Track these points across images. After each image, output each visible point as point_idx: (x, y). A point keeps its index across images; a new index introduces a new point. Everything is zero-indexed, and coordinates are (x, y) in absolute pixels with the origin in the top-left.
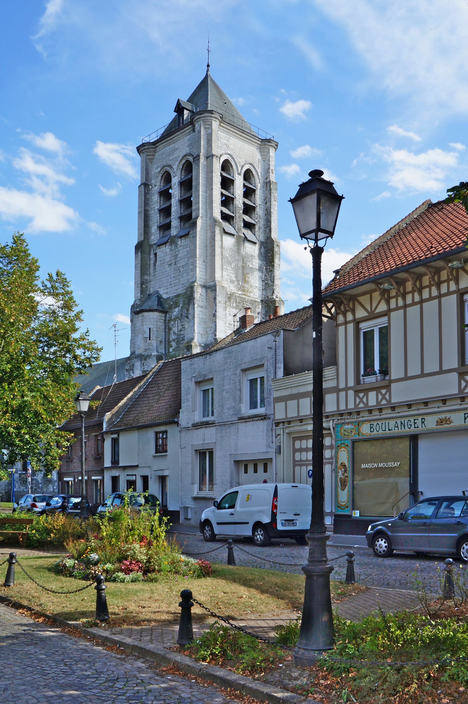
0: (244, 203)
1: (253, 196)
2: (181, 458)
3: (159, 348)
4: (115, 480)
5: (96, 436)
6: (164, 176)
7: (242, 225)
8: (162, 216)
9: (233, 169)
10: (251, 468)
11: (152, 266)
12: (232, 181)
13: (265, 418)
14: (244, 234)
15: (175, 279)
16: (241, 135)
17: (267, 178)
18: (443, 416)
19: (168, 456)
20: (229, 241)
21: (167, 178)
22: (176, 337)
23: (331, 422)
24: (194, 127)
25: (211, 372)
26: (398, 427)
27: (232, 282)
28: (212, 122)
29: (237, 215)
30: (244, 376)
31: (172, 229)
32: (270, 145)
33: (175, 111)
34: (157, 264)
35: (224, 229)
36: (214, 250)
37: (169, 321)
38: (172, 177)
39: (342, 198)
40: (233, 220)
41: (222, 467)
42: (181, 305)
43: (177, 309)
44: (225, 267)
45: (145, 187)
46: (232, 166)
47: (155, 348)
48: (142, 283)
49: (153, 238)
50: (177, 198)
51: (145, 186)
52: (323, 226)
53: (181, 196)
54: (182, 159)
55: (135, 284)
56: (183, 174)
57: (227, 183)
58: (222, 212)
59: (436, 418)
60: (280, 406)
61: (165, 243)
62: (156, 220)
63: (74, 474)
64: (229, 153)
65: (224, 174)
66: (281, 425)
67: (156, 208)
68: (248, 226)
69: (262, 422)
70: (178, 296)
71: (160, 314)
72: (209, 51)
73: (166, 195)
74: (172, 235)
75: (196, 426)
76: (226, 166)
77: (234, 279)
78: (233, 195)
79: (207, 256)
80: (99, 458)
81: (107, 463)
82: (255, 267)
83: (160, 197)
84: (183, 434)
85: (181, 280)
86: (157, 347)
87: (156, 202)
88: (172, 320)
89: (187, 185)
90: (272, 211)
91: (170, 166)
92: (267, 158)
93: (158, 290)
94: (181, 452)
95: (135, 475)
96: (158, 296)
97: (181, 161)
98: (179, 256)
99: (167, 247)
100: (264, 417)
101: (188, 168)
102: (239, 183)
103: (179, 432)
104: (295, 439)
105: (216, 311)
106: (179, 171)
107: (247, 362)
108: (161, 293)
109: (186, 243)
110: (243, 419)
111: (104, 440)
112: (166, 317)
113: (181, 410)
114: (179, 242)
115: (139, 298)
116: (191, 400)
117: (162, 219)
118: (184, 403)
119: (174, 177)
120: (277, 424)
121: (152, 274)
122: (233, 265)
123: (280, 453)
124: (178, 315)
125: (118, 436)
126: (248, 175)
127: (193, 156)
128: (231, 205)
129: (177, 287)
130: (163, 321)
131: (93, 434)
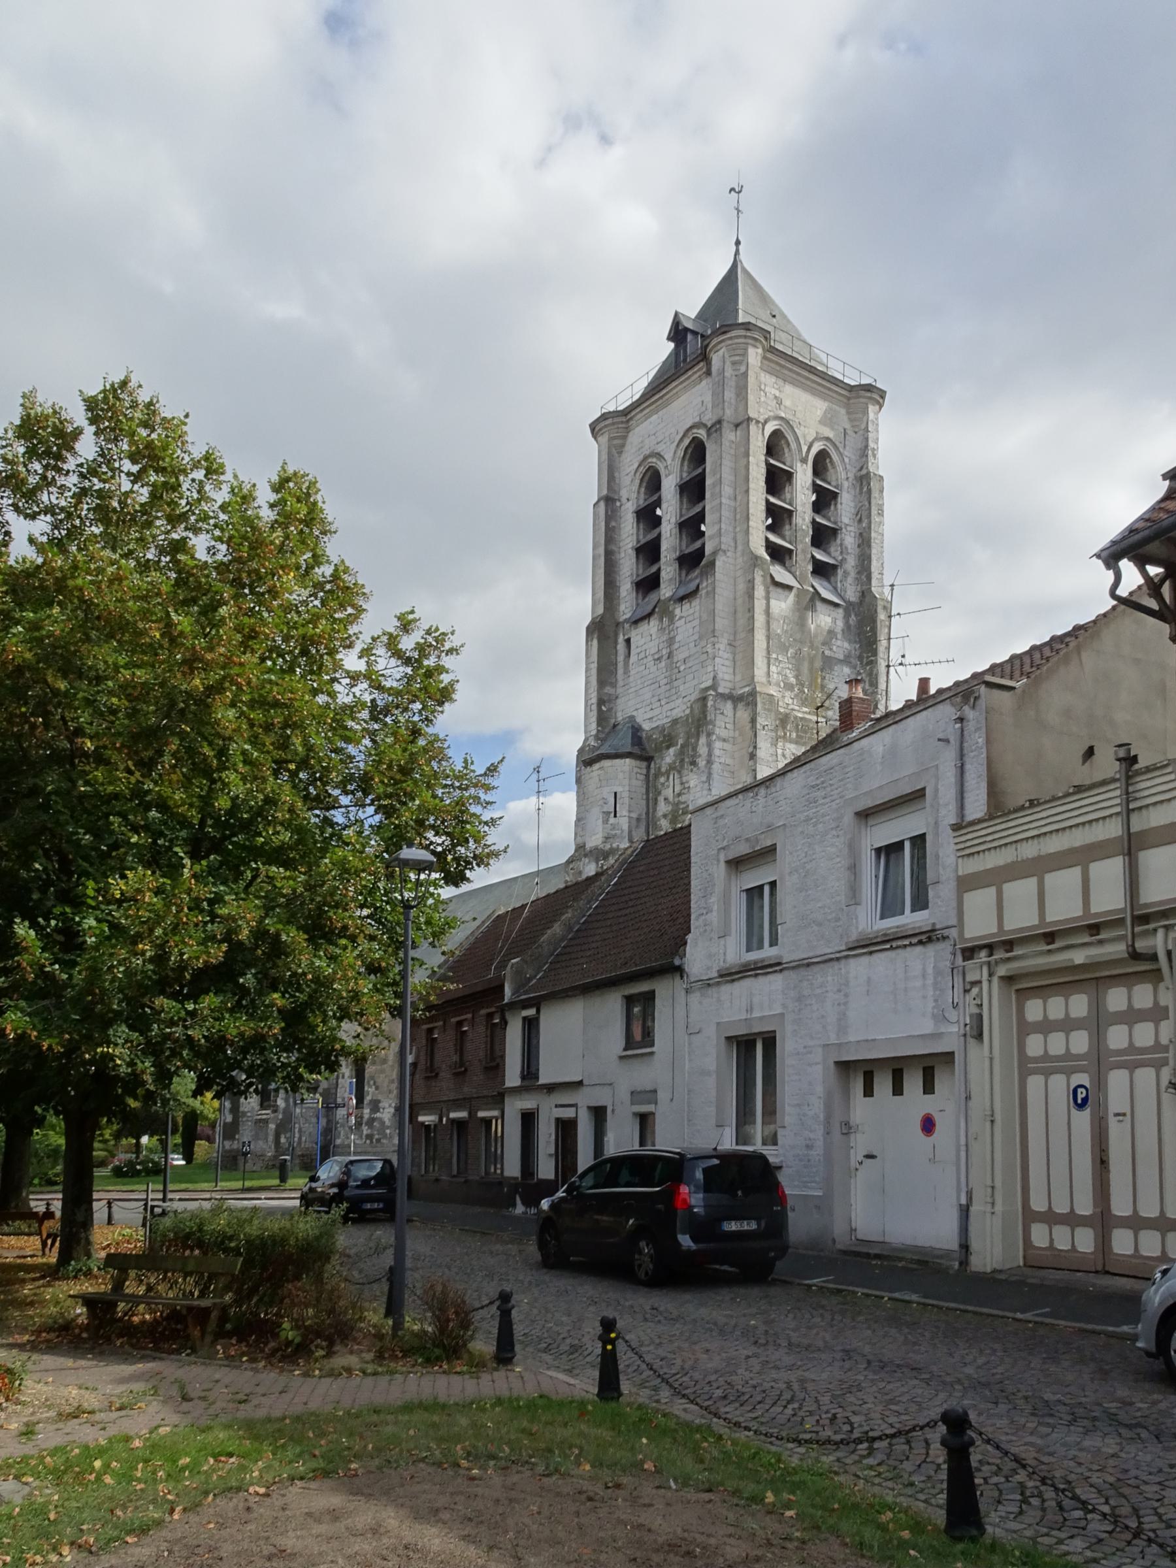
0: (814, 522)
1: (832, 507)
2: (690, 1060)
3: (634, 833)
4: (529, 1120)
5: (490, 1016)
6: (647, 478)
7: (810, 568)
8: (641, 561)
9: (790, 450)
10: (883, 1085)
11: (620, 665)
12: (789, 476)
13: (930, 940)
14: (813, 586)
15: (668, 687)
16: (808, 379)
17: (861, 468)
19: (656, 1057)
20: (782, 605)
21: (652, 481)
22: (670, 808)
23: (1160, 934)
24: (709, 364)
25: (770, 829)
27: (789, 687)
28: (746, 349)
29: (800, 547)
30: (863, 832)
31: (662, 586)
32: (870, 398)
33: (669, 339)
34: (632, 660)
35: (772, 577)
36: (752, 618)
37: (656, 776)
38: (663, 477)
40: (791, 558)
41: (803, 1077)
42: (680, 741)
43: (672, 751)
44: (774, 656)
45: (606, 506)
46: (788, 445)
47: (626, 834)
48: (601, 702)
49: (622, 607)
50: (673, 520)
51: (609, 501)
53: (681, 516)
54: (684, 436)
56: (686, 468)
58: (767, 539)
60: (980, 902)
61: (648, 616)
62: (629, 568)
64: (783, 415)
66: (983, 953)
67: (630, 545)
68: (822, 570)
69: (919, 949)
70: (675, 722)
71: (638, 763)
72: (739, 211)
73: (648, 516)
74: (662, 598)
75: (731, 975)
76: (774, 445)
77: (793, 680)
79: (735, 634)
80: (495, 1066)
81: (513, 1078)
82: (836, 656)
83: (638, 522)
84: (695, 998)
85: (681, 688)
86: (630, 832)
87: (629, 533)
88: (663, 775)
89: (694, 489)
90: (873, 535)
91: (659, 456)
92: (863, 427)
93: (634, 713)
94: (690, 1044)
95: (575, 1105)
96: (633, 727)
97: (681, 440)
98: (677, 639)
99: (652, 623)
100: (928, 937)
101: (697, 453)
102: (803, 476)
103: (683, 993)
104: (1024, 994)
105: (755, 747)
106: (678, 462)
107: (878, 784)
108: (638, 720)
109: (691, 611)
110: (869, 945)
111: (506, 1023)
112: (648, 768)
113: (689, 938)
114: (677, 611)
115: (594, 732)
116: (715, 908)
117: (641, 566)
118: (697, 919)
119: (666, 476)
120: (969, 953)
121: (620, 683)
122: (791, 651)
123: (979, 1036)
124: (674, 763)
125: (538, 1011)
126: (821, 464)
127: (705, 425)
128: (787, 527)
129: (672, 705)
130: (643, 777)
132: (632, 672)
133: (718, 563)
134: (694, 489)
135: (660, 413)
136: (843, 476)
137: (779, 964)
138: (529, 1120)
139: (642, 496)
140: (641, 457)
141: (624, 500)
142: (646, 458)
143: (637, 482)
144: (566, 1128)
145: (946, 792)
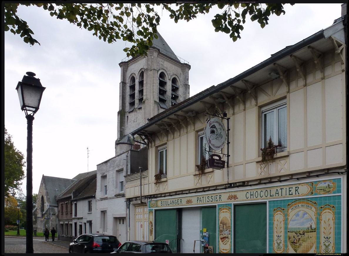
4: (76, 224)
9: (166, 77)
11: (126, 122)
12: (166, 83)
18: (188, 199)
21: (133, 79)
26: (278, 194)
32: (187, 67)
38: (136, 79)
39: (44, 88)
40: (166, 102)
49: (126, 108)
50: (138, 90)
51: (123, 83)
52: (26, 104)
53: (140, 89)
55: (118, 131)
57: (162, 84)
59: (186, 200)
62: (128, 100)
63: (63, 220)
65: (161, 79)
67: (128, 94)
71: (129, 145)
73: (133, 88)
78: (166, 90)
81: (73, 217)
87: (128, 91)
89: (141, 83)
91: (135, 74)
96: (128, 137)
106: (139, 76)
111: (72, 204)
119: (136, 79)
126: (174, 81)
128: (165, 95)
131: (61, 203)
132: (128, 124)
133: (146, 102)
134: (141, 83)
135: (135, 64)
136: (180, 84)
137: (107, 198)
138: (76, 224)
139: (131, 83)
140: (131, 74)
141: (127, 83)
142: (132, 74)
143: (130, 79)
144: (81, 226)
145: (125, 169)
